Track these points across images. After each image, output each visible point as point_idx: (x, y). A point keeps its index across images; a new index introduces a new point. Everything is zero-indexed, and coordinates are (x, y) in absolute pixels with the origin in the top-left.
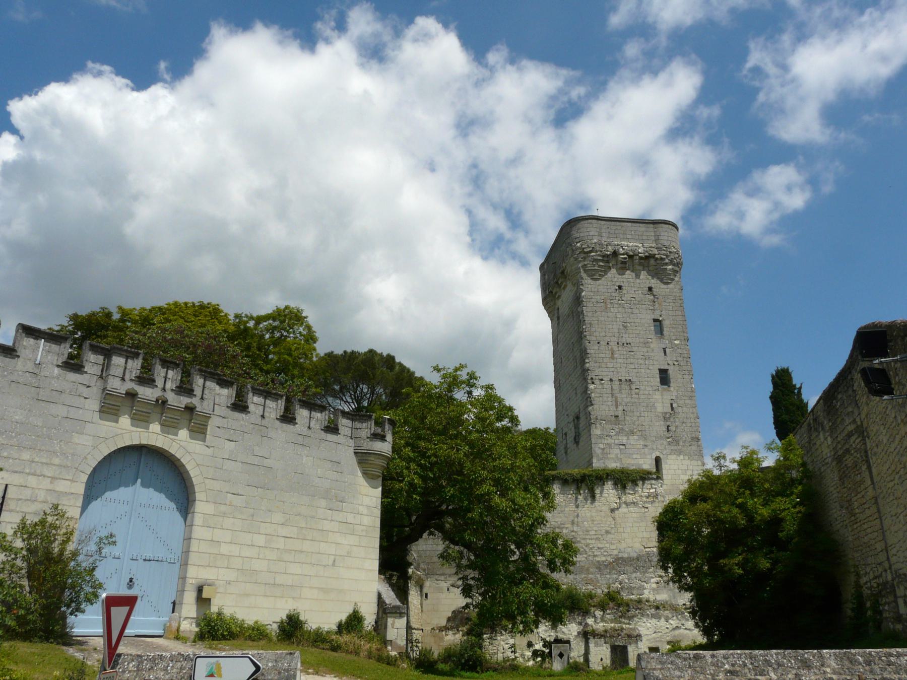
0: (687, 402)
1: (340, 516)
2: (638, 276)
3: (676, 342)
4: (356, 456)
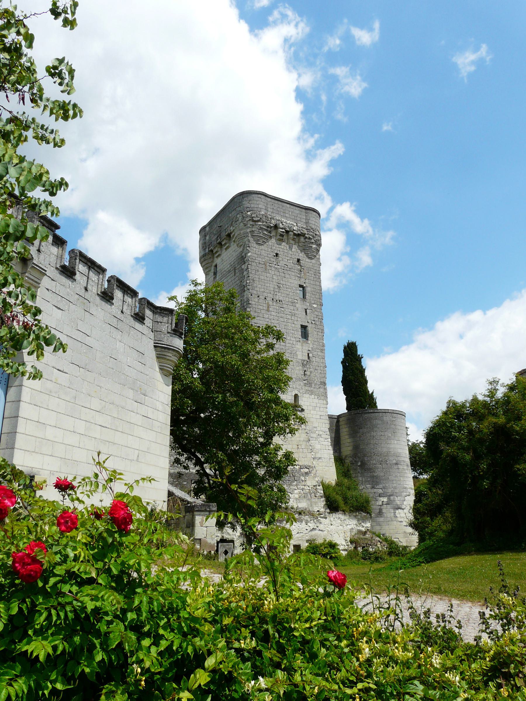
0: (319, 353)
1: (143, 410)
2: (291, 248)
3: (315, 306)
4: (156, 351)
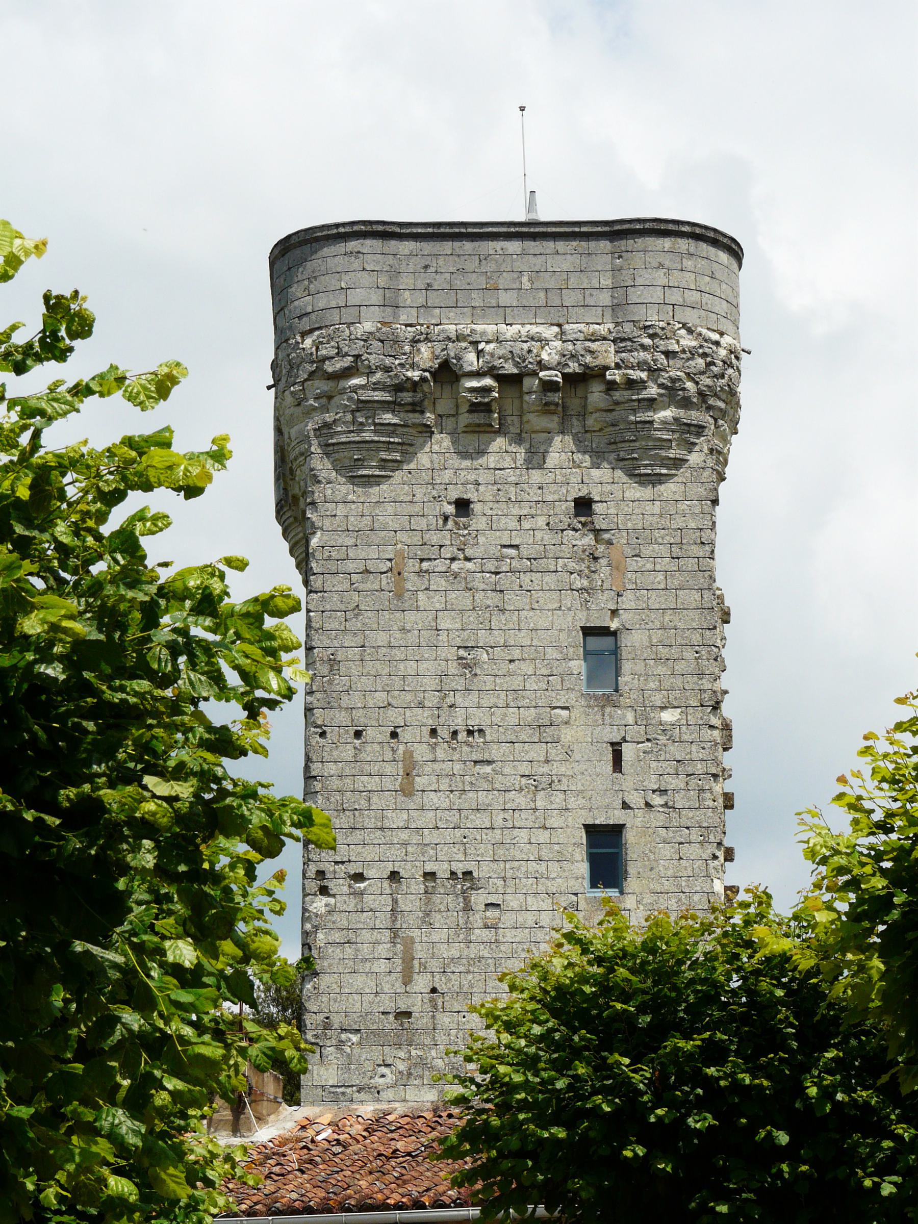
2: (536, 459)
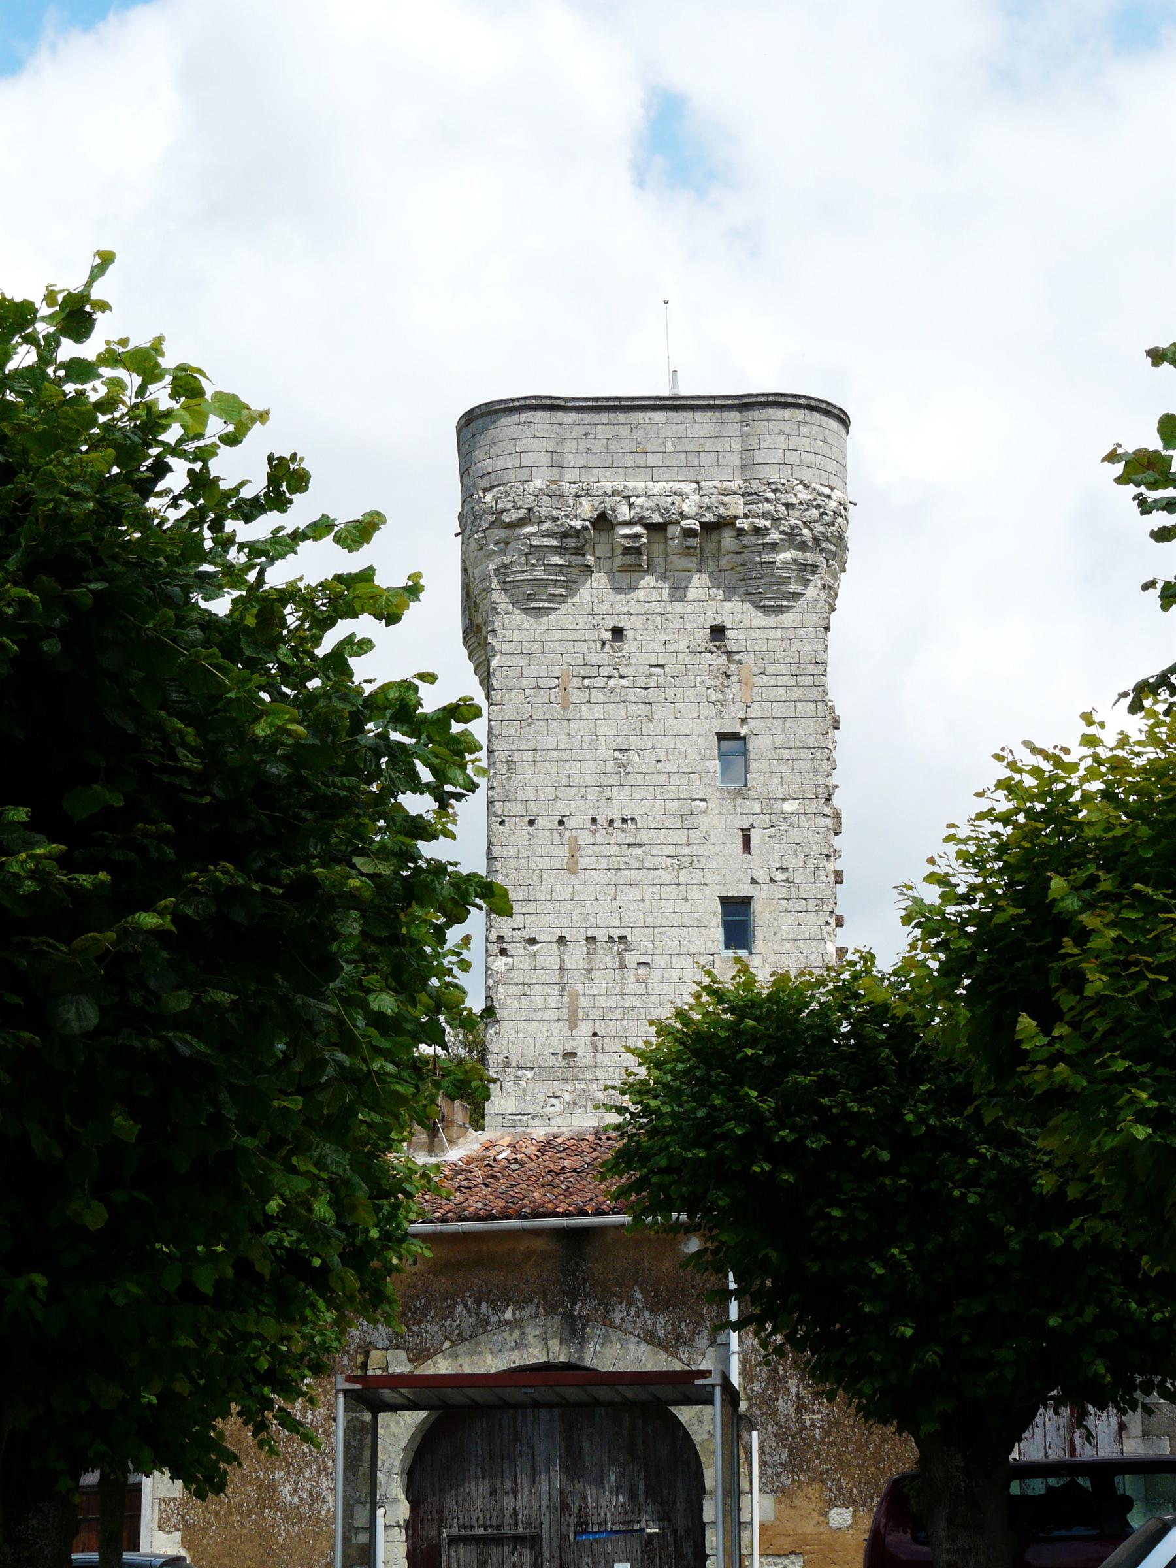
2: (678, 593)
